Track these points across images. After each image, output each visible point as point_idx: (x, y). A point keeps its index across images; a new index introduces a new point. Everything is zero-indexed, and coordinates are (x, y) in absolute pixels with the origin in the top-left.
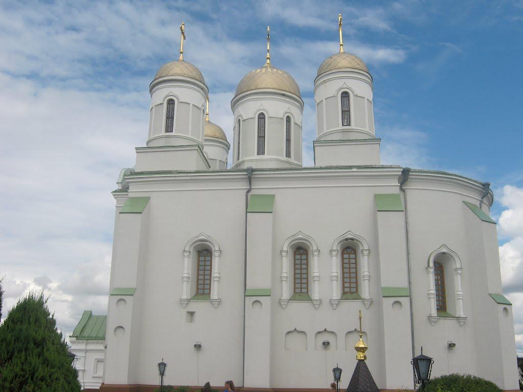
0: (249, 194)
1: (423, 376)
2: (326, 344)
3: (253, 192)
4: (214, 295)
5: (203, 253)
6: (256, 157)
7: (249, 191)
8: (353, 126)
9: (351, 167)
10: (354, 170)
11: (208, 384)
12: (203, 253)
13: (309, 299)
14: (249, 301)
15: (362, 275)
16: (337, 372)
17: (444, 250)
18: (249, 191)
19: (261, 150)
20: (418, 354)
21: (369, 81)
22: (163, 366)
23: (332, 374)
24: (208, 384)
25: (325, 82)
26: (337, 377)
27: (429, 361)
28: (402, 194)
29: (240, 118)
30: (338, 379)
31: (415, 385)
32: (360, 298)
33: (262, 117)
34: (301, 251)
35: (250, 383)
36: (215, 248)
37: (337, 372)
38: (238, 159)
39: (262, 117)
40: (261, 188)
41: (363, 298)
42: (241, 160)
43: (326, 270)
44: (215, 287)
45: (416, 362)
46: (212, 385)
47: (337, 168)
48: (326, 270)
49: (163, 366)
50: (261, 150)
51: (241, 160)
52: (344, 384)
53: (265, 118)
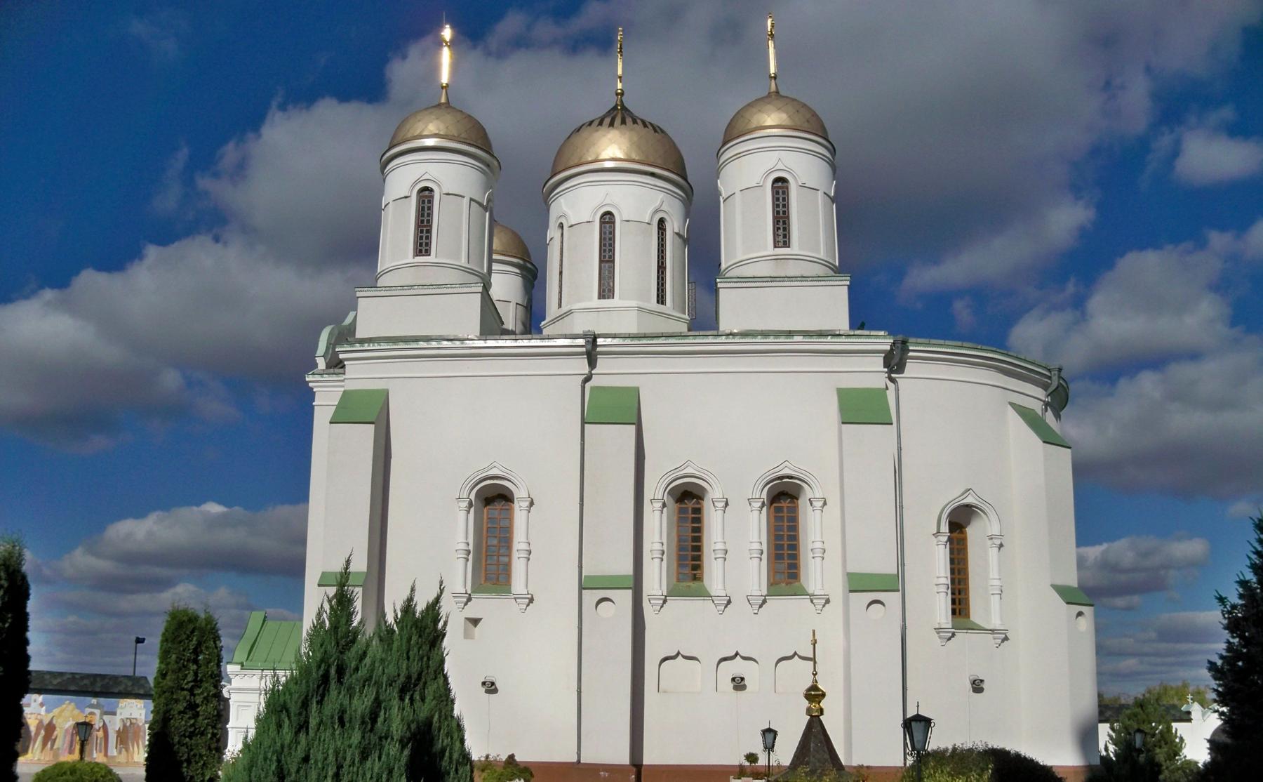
0: (588, 385)
1: (918, 746)
2: (739, 684)
3: (595, 382)
4: (518, 585)
5: (494, 498)
6: (596, 302)
7: (588, 379)
8: (795, 248)
9: (790, 334)
10: (797, 339)
11: (512, 757)
12: (494, 498)
13: (704, 594)
14: (591, 597)
15: (810, 547)
16: (769, 735)
17: (970, 500)
18: (588, 379)
19: (606, 291)
20: (911, 713)
21: (828, 155)
22: (772, 735)
23: (760, 738)
24: (512, 757)
25: (738, 156)
26: (769, 745)
27: (927, 722)
28: (891, 385)
29: (563, 220)
30: (769, 747)
31: (905, 759)
32: (803, 593)
33: (607, 219)
34: (688, 497)
35: (590, 756)
36: (519, 493)
37: (769, 735)
38: (560, 306)
39: (607, 219)
40: (611, 373)
41: (810, 592)
42: (565, 308)
43: (737, 535)
44: (518, 567)
45: (908, 724)
46: (518, 758)
47: (765, 334)
48: (737, 535)
49: (772, 735)
50: (606, 291)
51: (565, 308)
52: (784, 754)
53: (614, 223)
